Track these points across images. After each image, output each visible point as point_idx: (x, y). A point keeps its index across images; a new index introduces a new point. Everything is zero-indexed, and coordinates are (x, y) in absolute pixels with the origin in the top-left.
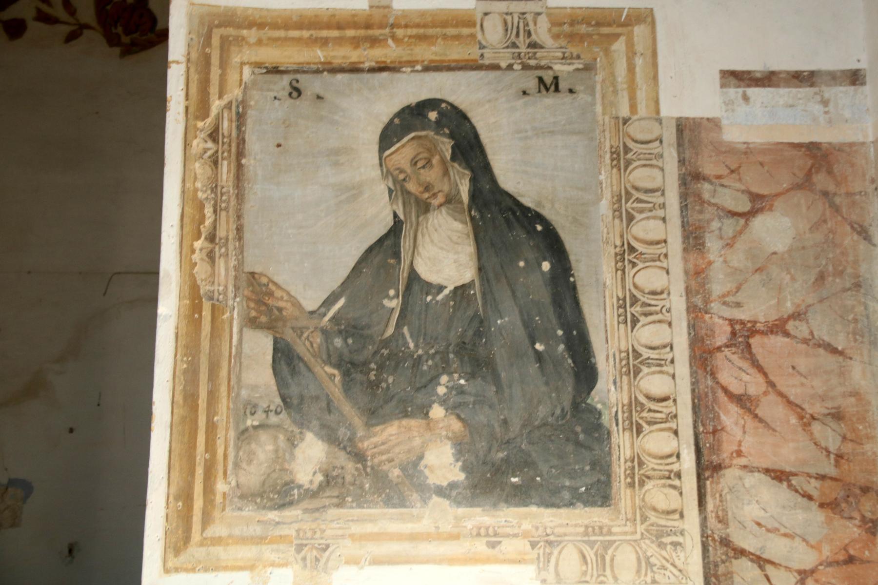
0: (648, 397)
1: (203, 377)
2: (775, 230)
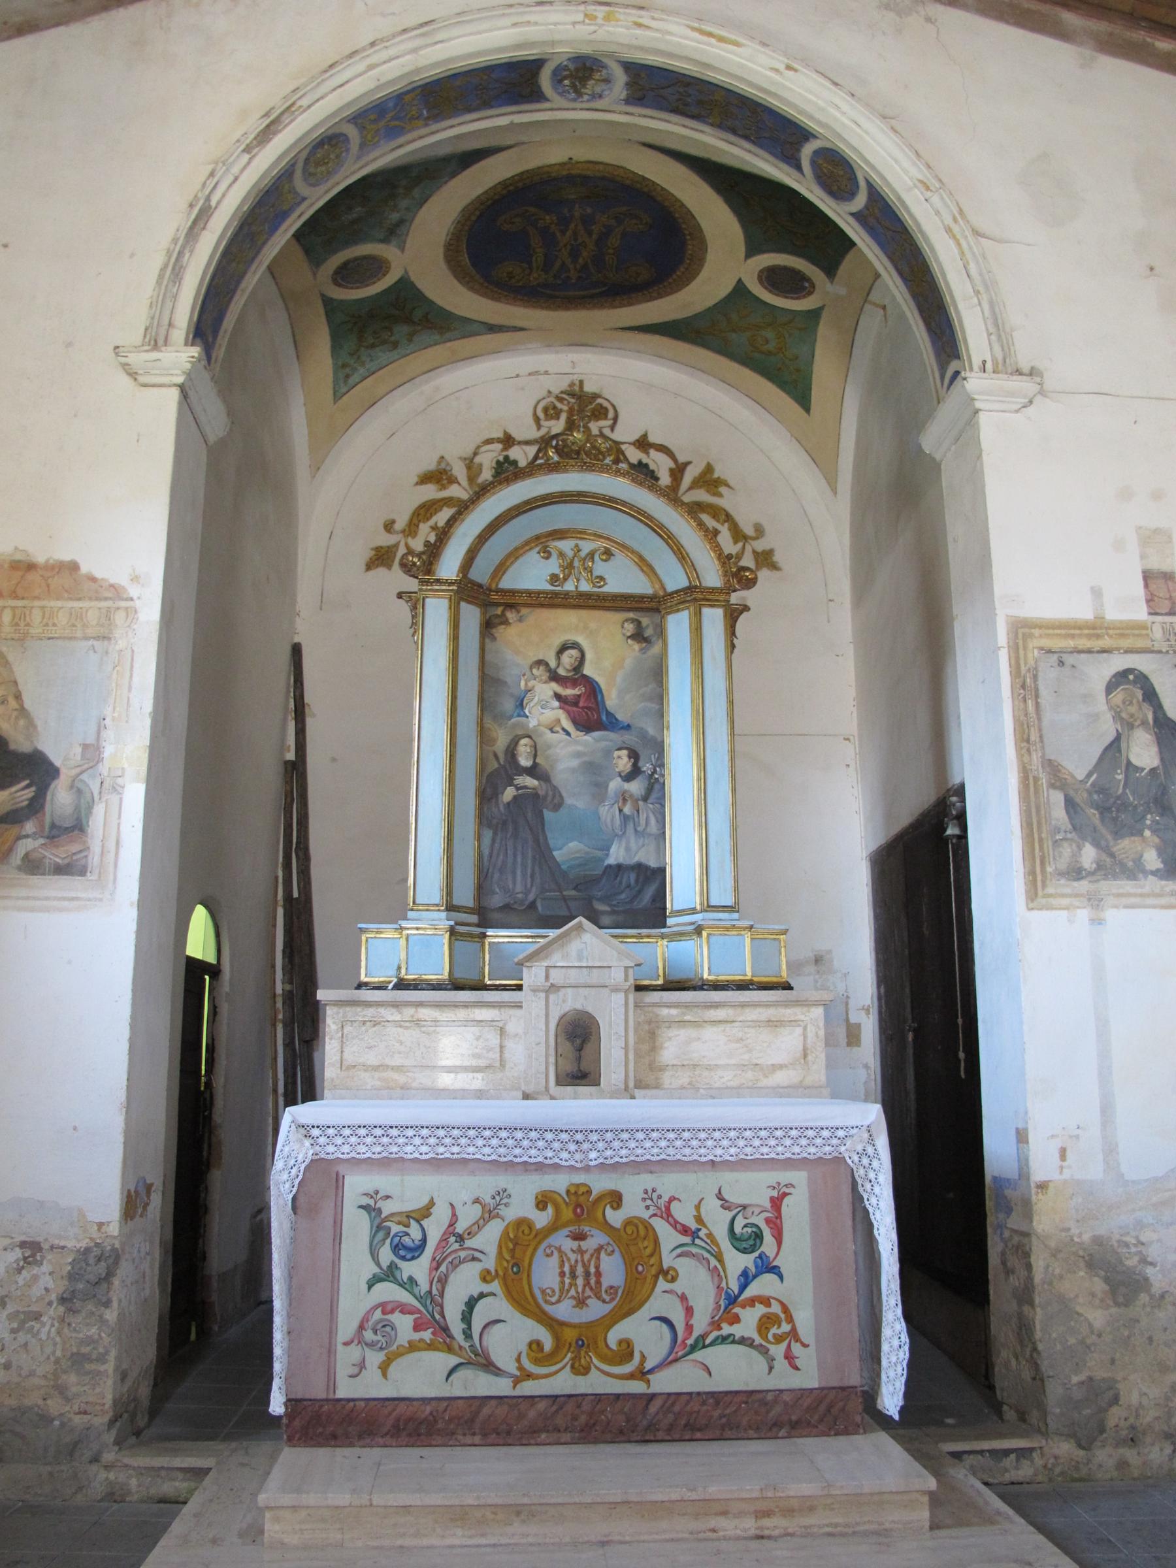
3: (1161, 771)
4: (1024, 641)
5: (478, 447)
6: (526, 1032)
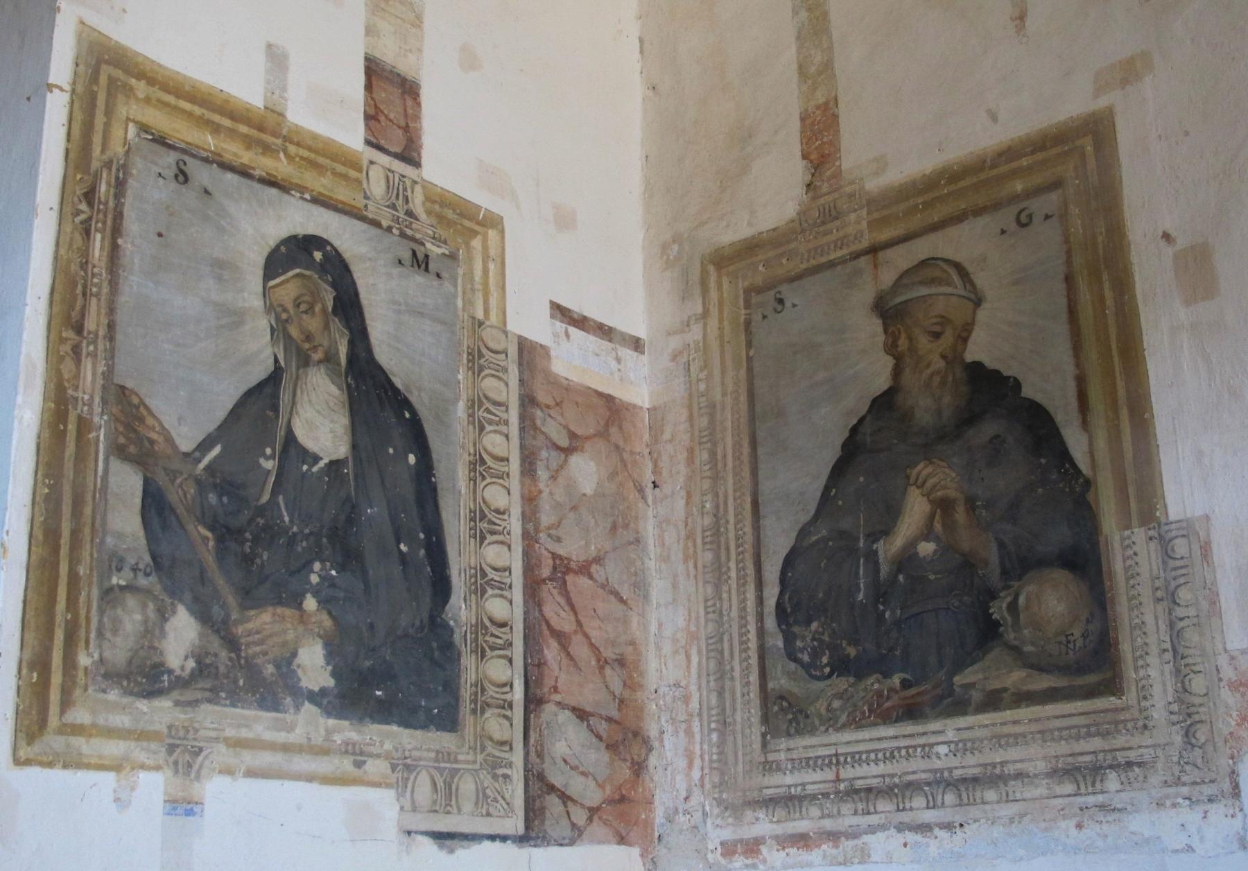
0: (491, 620)
1: (66, 509)
2: (586, 471)
3: (349, 470)
4: (111, 95)
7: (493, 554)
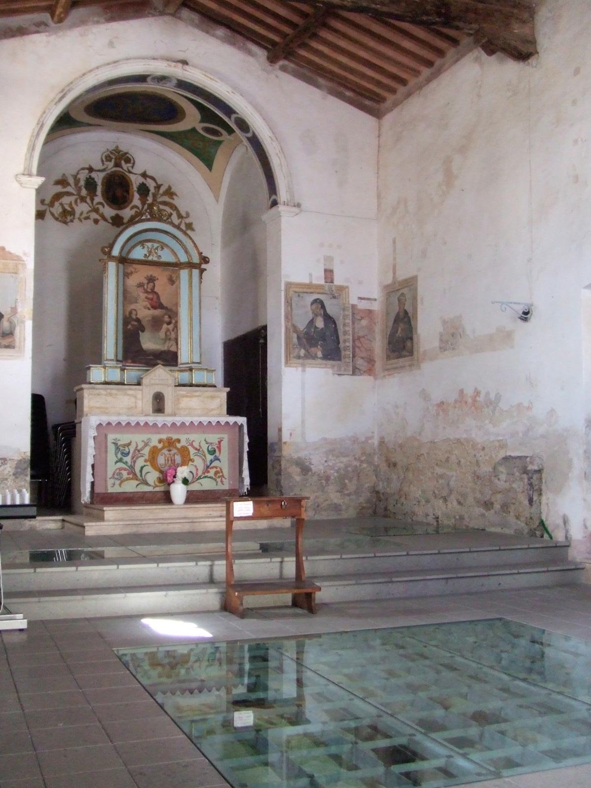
2: (364, 322)
5: (79, 171)
6: (142, 398)
7: (347, 337)
